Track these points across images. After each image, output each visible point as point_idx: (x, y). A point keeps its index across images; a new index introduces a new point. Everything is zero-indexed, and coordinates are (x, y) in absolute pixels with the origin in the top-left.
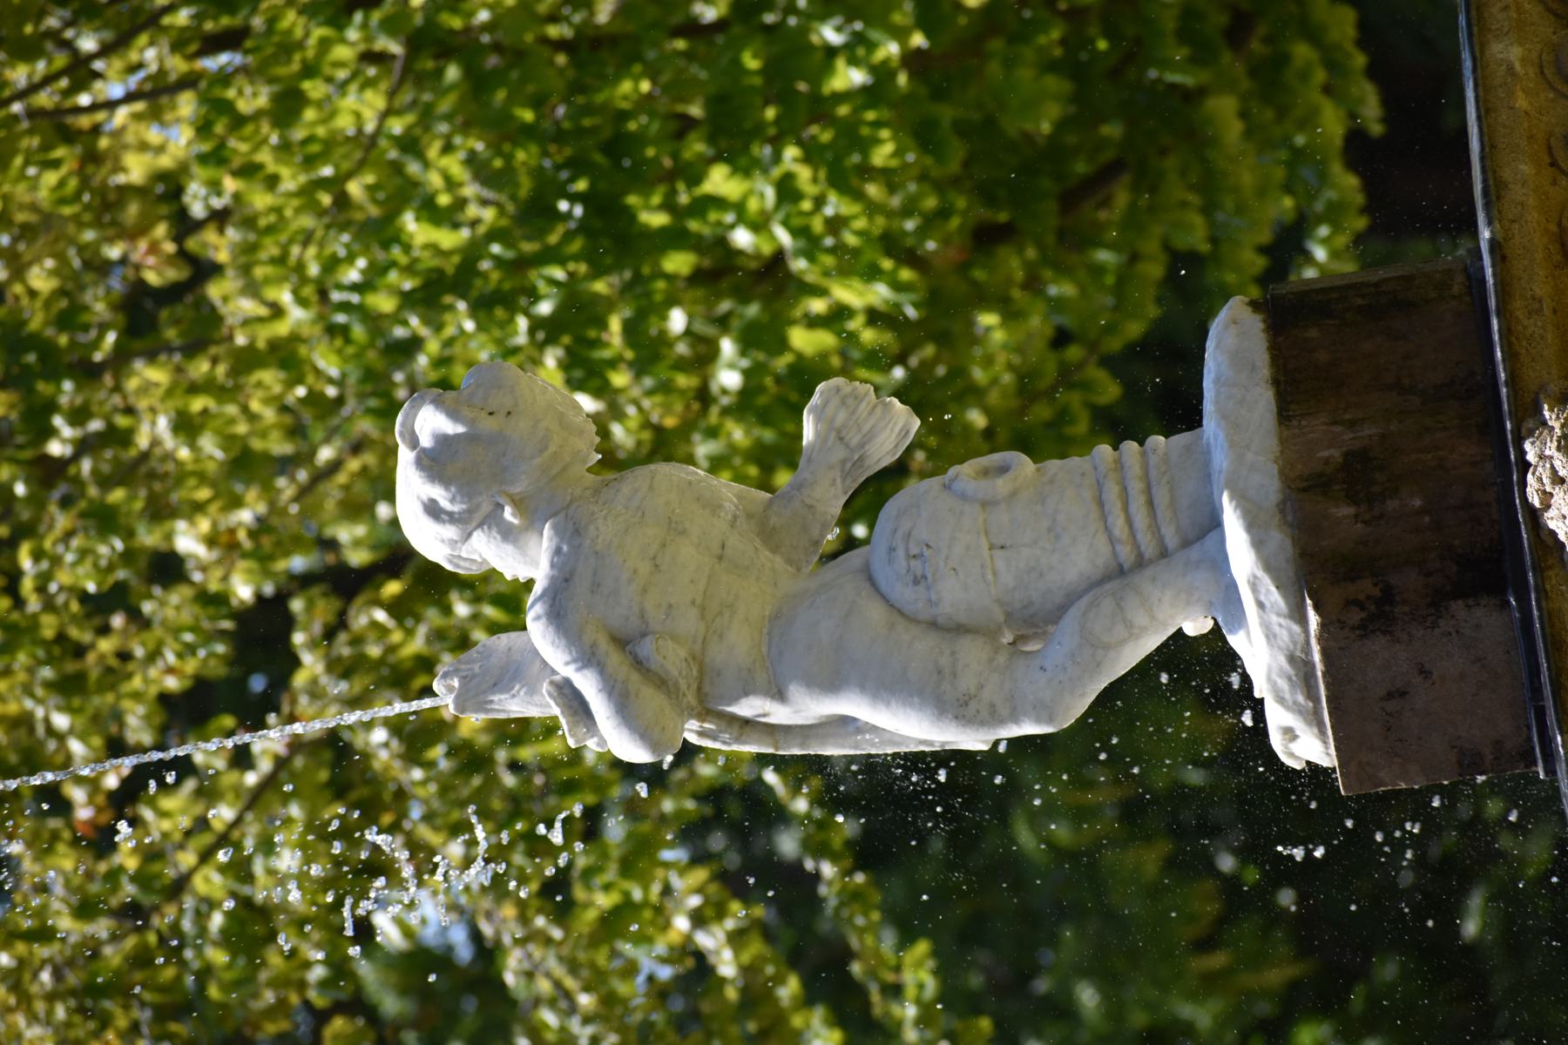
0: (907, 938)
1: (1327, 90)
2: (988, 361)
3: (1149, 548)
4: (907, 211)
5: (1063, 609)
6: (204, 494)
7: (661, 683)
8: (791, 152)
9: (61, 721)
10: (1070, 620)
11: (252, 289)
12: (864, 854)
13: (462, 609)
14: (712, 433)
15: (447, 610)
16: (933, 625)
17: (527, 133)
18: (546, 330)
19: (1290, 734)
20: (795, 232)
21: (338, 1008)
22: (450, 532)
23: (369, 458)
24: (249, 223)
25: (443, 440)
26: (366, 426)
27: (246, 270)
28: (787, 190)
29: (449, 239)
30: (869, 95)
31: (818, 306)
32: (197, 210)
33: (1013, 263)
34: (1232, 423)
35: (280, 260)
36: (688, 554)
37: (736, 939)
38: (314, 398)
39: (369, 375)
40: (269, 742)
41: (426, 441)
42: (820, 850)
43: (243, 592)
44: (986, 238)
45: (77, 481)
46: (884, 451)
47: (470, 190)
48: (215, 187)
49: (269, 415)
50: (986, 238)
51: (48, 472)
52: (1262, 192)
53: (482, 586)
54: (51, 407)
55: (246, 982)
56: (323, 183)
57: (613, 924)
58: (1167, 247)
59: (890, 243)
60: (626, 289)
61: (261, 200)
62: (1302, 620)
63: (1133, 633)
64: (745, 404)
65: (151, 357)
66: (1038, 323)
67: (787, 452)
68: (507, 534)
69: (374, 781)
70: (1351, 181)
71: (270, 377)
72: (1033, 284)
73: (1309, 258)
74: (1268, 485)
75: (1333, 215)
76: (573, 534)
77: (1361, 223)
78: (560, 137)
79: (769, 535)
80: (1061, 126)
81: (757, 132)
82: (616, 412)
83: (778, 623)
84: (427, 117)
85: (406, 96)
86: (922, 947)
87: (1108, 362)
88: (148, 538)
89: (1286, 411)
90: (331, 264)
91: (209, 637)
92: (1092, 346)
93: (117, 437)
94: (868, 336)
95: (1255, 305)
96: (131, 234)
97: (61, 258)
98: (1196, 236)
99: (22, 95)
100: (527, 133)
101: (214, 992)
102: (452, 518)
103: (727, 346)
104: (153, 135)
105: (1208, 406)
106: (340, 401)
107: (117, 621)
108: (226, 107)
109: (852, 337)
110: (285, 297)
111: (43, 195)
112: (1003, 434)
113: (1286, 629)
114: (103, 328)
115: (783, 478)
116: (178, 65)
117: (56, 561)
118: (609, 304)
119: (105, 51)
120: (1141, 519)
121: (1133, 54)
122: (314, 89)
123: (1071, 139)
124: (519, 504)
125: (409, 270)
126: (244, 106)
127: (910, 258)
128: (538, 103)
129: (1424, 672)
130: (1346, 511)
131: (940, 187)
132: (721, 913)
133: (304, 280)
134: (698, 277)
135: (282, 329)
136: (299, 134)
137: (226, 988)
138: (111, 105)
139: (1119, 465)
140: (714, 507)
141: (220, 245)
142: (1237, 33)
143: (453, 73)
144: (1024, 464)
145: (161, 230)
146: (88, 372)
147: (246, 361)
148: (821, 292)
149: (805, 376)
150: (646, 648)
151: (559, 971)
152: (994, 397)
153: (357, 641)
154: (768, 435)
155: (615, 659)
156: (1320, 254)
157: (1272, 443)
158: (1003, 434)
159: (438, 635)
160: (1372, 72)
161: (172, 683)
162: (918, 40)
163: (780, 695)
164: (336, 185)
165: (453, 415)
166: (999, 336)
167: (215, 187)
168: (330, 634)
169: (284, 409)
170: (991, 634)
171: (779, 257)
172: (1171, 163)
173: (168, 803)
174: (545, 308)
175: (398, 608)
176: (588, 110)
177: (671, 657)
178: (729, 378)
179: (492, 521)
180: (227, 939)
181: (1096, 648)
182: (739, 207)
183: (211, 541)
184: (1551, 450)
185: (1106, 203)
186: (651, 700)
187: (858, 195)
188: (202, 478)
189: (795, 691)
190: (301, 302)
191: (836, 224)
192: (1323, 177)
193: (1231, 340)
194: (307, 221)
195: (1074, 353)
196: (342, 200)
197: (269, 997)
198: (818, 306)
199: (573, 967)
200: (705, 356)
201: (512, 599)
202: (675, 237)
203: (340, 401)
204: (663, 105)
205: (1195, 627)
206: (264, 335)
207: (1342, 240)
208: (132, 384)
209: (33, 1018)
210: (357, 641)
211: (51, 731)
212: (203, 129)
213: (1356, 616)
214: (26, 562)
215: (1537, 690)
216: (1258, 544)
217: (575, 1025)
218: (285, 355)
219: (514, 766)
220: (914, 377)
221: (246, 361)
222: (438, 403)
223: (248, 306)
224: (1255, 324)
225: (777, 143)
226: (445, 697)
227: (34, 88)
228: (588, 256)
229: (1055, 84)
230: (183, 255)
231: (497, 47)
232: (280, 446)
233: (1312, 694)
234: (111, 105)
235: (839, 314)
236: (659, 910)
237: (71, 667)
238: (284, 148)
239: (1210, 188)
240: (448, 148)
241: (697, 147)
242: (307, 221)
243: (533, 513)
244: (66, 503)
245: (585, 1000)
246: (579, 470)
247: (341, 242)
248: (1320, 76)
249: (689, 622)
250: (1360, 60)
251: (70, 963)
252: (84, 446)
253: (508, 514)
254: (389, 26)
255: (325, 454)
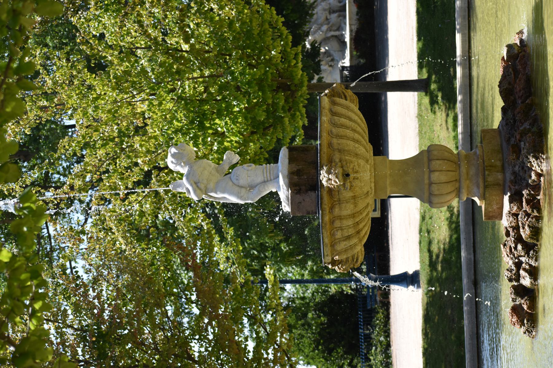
0: (231, 226)
1: (301, 119)
2: (251, 150)
3: (269, 179)
4: (242, 128)
5: (256, 186)
6: (142, 155)
7: (200, 189)
8: (227, 118)
9: (120, 183)
10: (258, 187)
11: (152, 128)
12: (226, 214)
13: (175, 175)
14: (212, 155)
15: (173, 175)
16: (238, 186)
17: (192, 111)
18: (191, 139)
19: (285, 206)
20: (227, 129)
21: (152, 226)
22: (174, 165)
23: (165, 153)
24: (153, 119)
25: (175, 153)
26: (165, 148)
27: (152, 126)
28: (226, 123)
29: (179, 124)
30: (239, 112)
31: (229, 140)
32: (146, 117)
33: (256, 137)
34: (282, 164)
35: (156, 125)
36: (206, 172)
37: (207, 224)
38: (158, 144)
39: (166, 142)
40: (147, 190)
41: (172, 153)
42: (220, 214)
43: (146, 169)
44: (253, 133)
45: (126, 151)
46: (235, 161)
47: (183, 118)
48: (149, 114)
49: (152, 145)
50: (253, 133)
51: (122, 150)
52: (291, 131)
53: (178, 173)
54: (124, 141)
55: (141, 221)
56: (163, 115)
57: (191, 220)
58: (277, 137)
59: (239, 132)
60: (203, 134)
61: (155, 116)
62: (288, 191)
63: (266, 190)
64: (217, 152)
65: (138, 136)
66: (258, 145)
67: (222, 159)
68: (182, 166)
69: (160, 196)
70: (303, 131)
71: (153, 140)
72: (258, 140)
73: (296, 141)
74: (286, 172)
75: (300, 135)
76: (191, 167)
77: (303, 137)
78: (196, 113)
79: (217, 171)
80: (264, 119)
81: (223, 115)
82: (199, 151)
83: (217, 183)
84: (179, 108)
85: (175, 105)
86: (232, 228)
87: (267, 152)
88: (134, 160)
89: (290, 163)
90: (163, 126)
91: (141, 175)
92: (265, 149)
93: (132, 146)
94: (235, 144)
95: (287, 148)
96: (137, 119)
97: (128, 121)
98: (281, 136)
99: (125, 99)
100: (192, 111)
101: (136, 222)
102: (175, 163)
103: (216, 144)
104: (142, 106)
105: (279, 161)
106: (162, 145)
107: (129, 171)
108: (152, 103)
109: (232, 144)
110: (156, 130)
111: (126, 112)
112: (251, 160)
113: (286, 192)
114: (132, 131)
115: (221, 162)
116: (146, 97)
117: (122, 162)
118: (200, 136)
119: (137, 94)
120: (268, 175)
121: (275, 111)
122: (164, 102)
123: (266, 121)
124: (184, 163)
125: (174, 128)
126: (154, 104)
127: (242, 135)
128: (194, 108)
129: (304, 200)
130: (296, 177)
131: (247, 125)
132: (205, 220)
133: (159, 128)
134: (213, 134)
135: (155, 134)
136: (161, 108)
137: (138, 222)
138: (137, 101)
139: (266, 167)
140: (210, 166)
141: (149, 122)
142: (289, 110)
143: (183, 102)
144: (253, 165)
145: (141, 119)
146: (129, 137)
147: (150, 138)
148: (229, 138)
149: (226, 149)
150: (199, 184)
151: (182, 226)
152: (251, 155)
153: (160, 177)
154: (220, 156)
155: (194, 185)
156: (298, 141)
157: (287, 167)
158: (251, 160)
159: (171, 178)
160: (307, 117)
161: (135, 180)
162: (246, 105)
163: (216, 193)
164: (165, 116)
165: (177, 149)
166: (253, 146)
167: (149, 114)
168: (157, 176)
169: (155, 145)
170: (246, 188)
171: (224, 132)
172: (279, 126)
173: (133, 196)
174: (191, 135)
175: (166, 174)
176: (201, 109)
177: (202, 186)
178: (215, 148)
179: (180, 164)
180: (139, 215)
181: (261, 192)
182: (219, 125)
183: (142, 162)
184: (324, 172)
185: (269, 130)
186: (198, 191)
187: (235, 125)
188: (142, 153)
189: (218, 193)
190: (159, 131)
191: (232, 129)
192: (299, 130)
193: (283, 152)
194: (161, 120)
195: (262, 150)
196: (166, 118)
197: (143, 224)
198: (229, 140)
199: (184, 225)
200: (212, 145)
201: (182, 175)
202: (210, 128)
203: (162, 145)
204: (211, 110)
205: (274, 190)
206: (153, 134)
207: (300, 139)
208: (135, 139)
209: (112, 222)
210: (160, 177)
211: (118, 184)
212: (149, 106)
213: (296, 192)
214: (118, 161)
215: (318, 204)
216: (284, 180)
217: (184, 233)
218: (155, 138)
219: (180, 197)
220: (240, 151)
221: (150, 138)
222: (175, 147)
223: (151, 131)
224: (287, 150)
225: (226, 117)
226: (171, 187)
227: (127, 98)
228: (198, 129)
229: (265, 114)
230: (144, 122)
231: (189, 99)
232: (154, 150)
233: (288, 201)
234: (137, 101)
235: (232, 141)
236: (197, 219)
237: (122, 176)
238: (159, 110)
239: (284, 130)
240: (181, 112)
241: (215, 116)
242: (161, 120)
243: (186, 164)
244: (124, 154)
245: (186, 230)
246: (193, 159)
247: (165, 123)
248: (300, 117)
249: (205, 182)
250: (305, 115)
251: (118, 216)
252: (127, 147)
253: (182, 164)
254: (175, 95)
255: (159, 151)
